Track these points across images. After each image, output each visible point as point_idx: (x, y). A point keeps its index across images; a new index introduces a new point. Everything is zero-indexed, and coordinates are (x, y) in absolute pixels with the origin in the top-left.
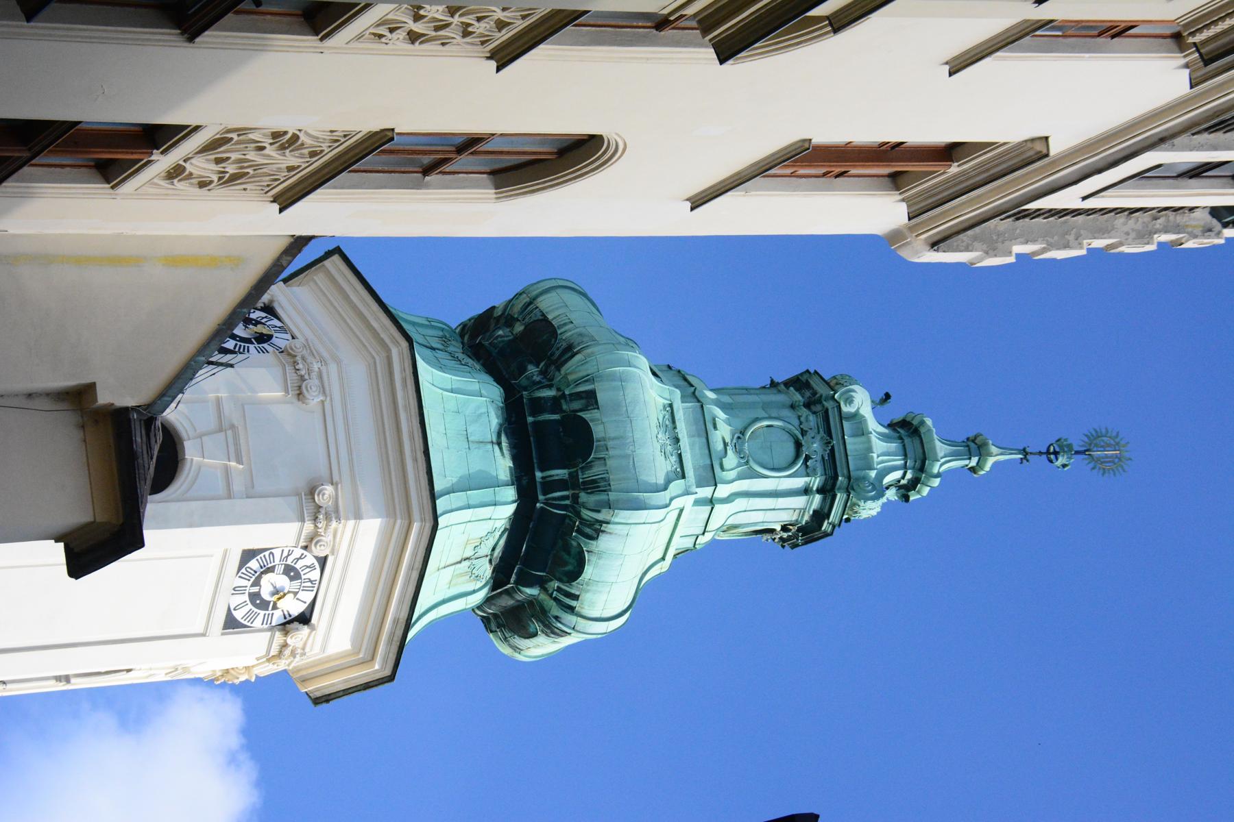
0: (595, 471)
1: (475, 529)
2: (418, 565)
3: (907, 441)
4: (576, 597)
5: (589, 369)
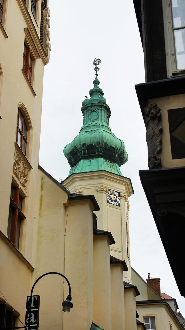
5: (79, 144)
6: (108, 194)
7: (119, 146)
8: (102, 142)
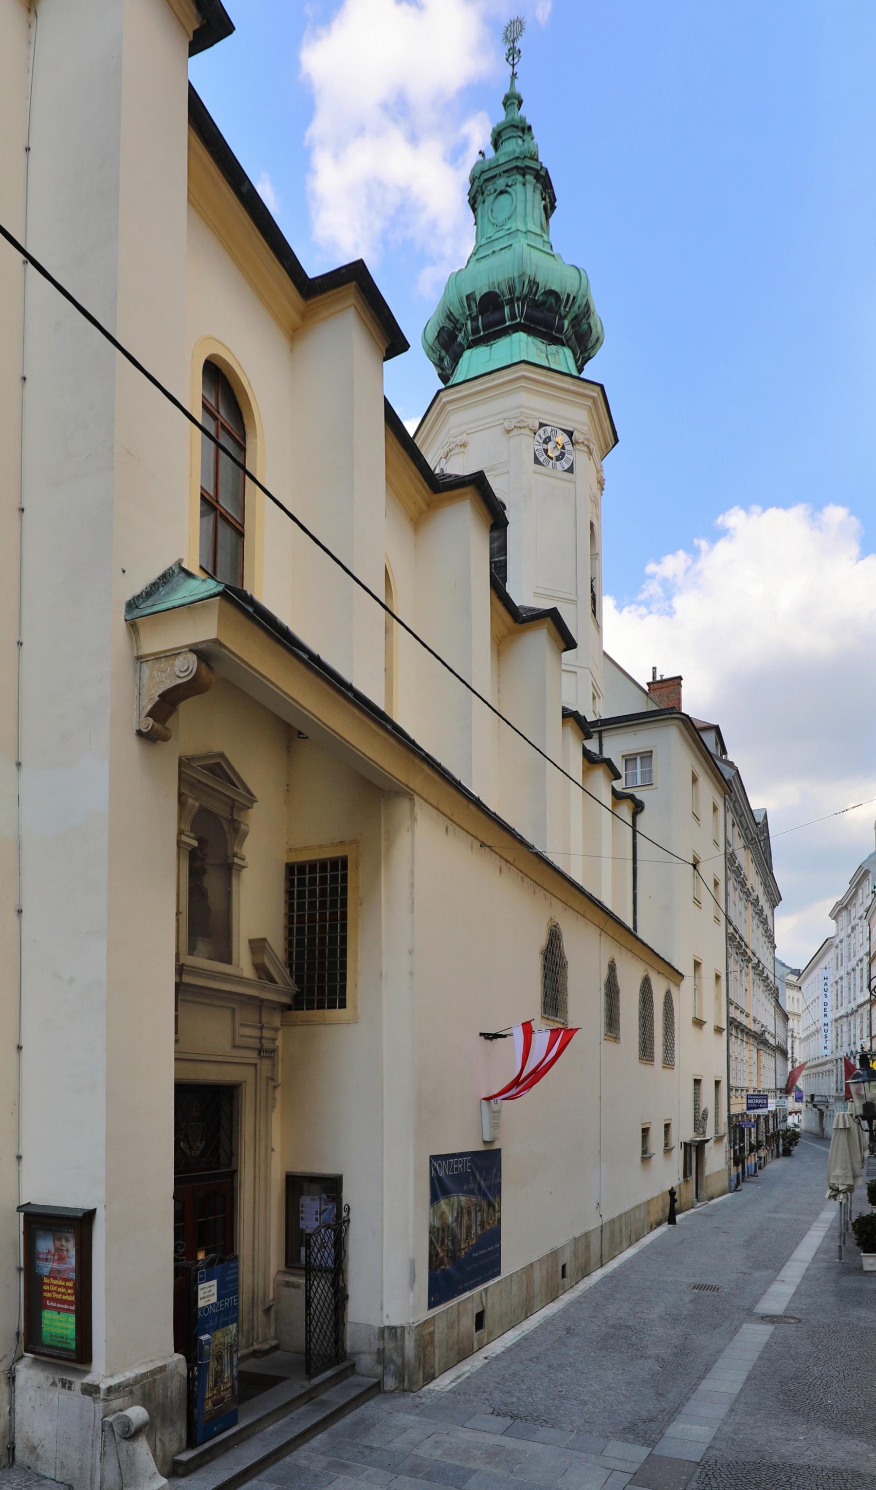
0: (504, 288)
3: (504, 138)
4: (569, 296)
6: (537, 437)
8: (520, 276)
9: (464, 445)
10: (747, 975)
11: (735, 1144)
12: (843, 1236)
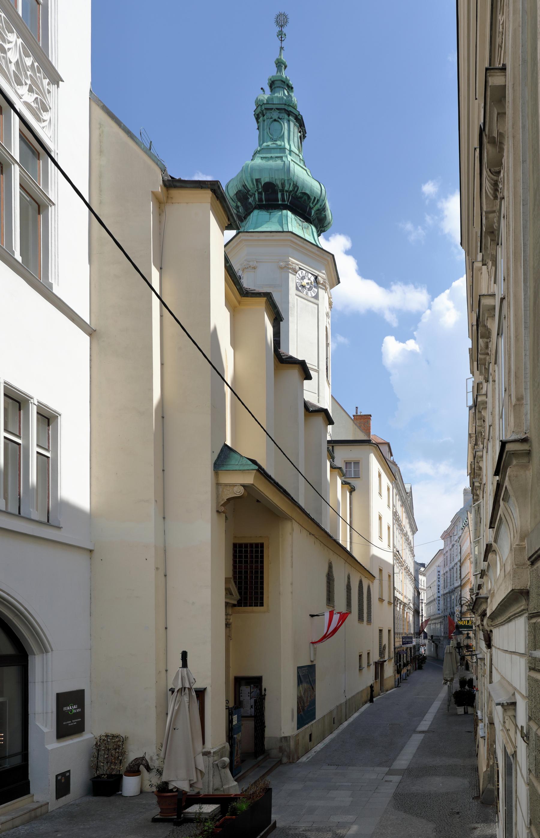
1: (293, 223)
2: (302, 240)
4: (315, 198)
7: (317, 193)
8: (288, 180)
9: (254, 268)
10: (402, 573)
11: (397, 663)
12: (449, 701)
